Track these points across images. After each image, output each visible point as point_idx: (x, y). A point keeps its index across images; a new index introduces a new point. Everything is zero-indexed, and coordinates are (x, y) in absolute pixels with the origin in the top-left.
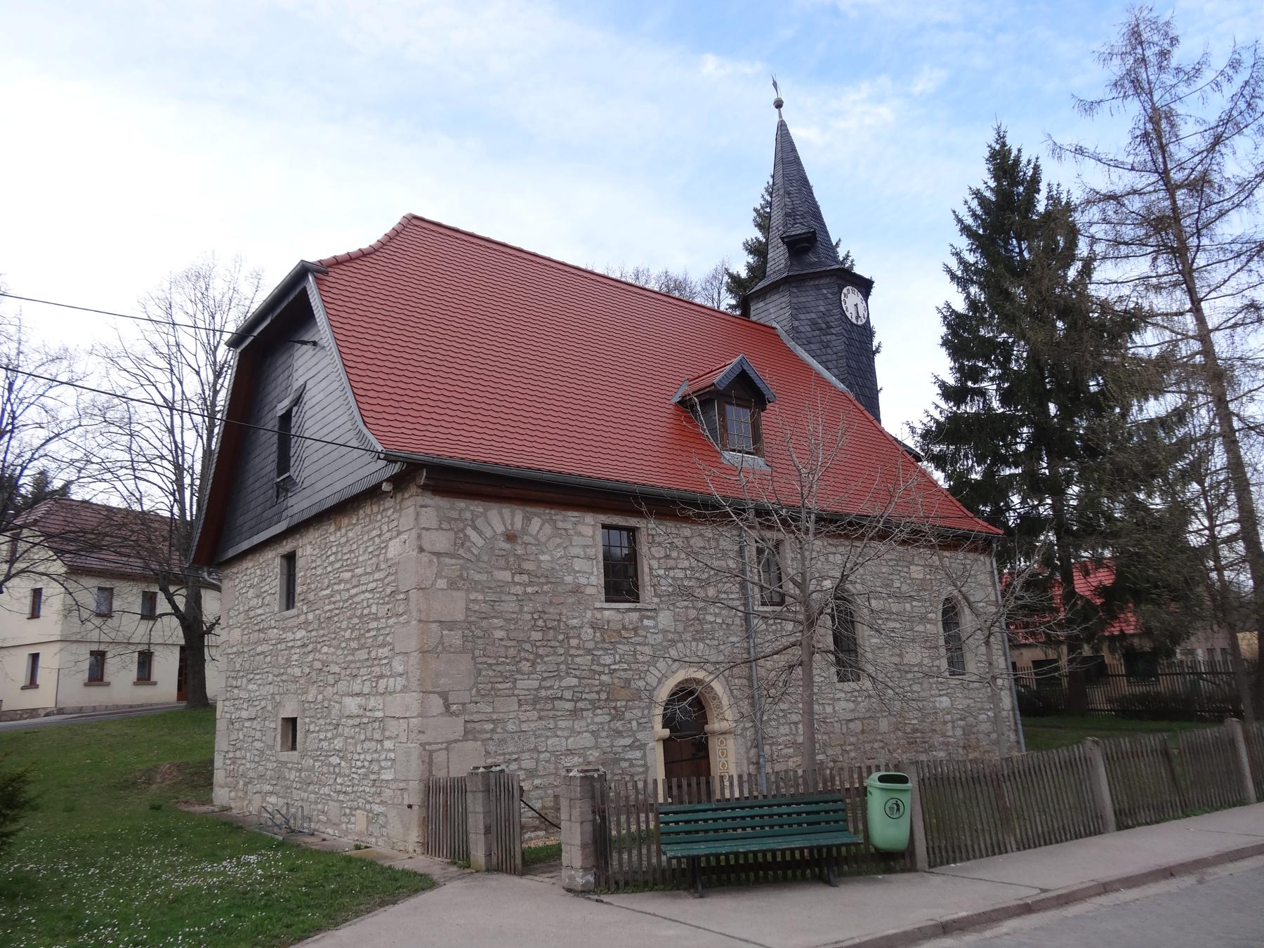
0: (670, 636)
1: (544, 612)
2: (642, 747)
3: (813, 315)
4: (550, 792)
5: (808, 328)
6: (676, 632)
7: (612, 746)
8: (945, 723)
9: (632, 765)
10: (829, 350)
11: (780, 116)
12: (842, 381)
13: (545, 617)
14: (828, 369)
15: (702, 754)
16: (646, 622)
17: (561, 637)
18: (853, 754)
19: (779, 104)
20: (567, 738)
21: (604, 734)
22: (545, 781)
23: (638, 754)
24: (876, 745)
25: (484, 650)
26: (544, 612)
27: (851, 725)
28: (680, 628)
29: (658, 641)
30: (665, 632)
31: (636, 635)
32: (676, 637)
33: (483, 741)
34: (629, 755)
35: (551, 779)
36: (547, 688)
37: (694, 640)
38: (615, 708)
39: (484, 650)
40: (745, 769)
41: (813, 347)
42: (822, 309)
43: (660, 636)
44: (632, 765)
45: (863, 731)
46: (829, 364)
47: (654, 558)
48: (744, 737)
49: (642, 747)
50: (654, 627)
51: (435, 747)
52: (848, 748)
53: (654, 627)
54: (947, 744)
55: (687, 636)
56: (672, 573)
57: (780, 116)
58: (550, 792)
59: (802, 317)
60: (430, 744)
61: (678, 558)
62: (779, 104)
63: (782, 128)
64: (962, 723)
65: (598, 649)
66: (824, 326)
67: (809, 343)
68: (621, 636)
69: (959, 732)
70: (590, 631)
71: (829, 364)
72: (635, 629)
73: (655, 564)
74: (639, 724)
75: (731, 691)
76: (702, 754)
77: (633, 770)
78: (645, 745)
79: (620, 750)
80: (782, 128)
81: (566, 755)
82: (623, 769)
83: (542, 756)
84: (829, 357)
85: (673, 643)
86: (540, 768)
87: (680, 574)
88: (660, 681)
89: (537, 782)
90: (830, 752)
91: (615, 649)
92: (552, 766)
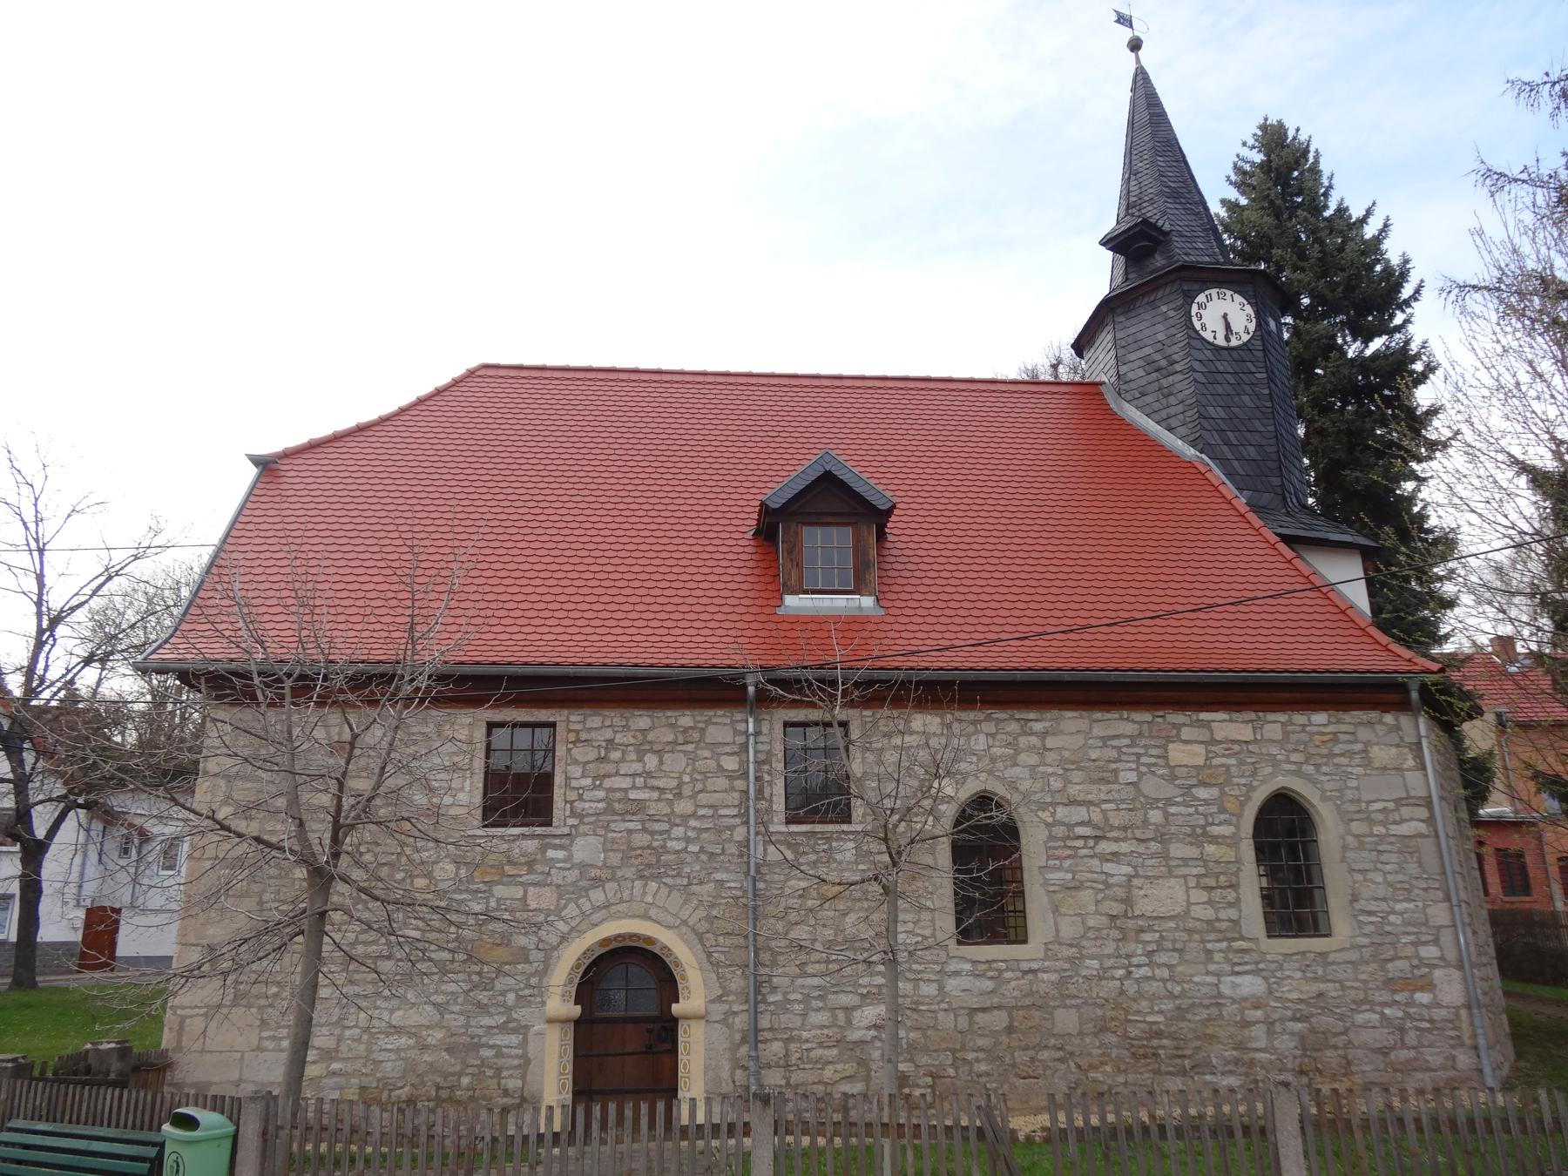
0: (593, 873)
1: (377, 844)
2: (523, 1030)
3: (1147, 351)
4: (355, 1081)
5: (1141, 372)
6: (605, 866)
7: (467, 1026)
8: (1247, 1024)
9: (499, 1054)
10: (1172, 400)
11: (1138, 60)
12: (1193, 444)
13: (378, 850)
14: (1170, 430)
15: (667, 1046)
16: (551, 853)
17: (400, 876)
18: (983, 1067)
19: (1135, 45)
20: (392, 1011)
21: (456, 1008)
22: (349, 1067)
23: (514, 1039)
24: (1045, 1055)
25: (278, 892)
26: (377, 844)
27: (981, 1018)
28: (615, 858)
29: (569, 880)
30: (583, 867)
31: (531, 871)
32: (605, 874)
33: (259, 1008)
34: (498, 1040)
35: (358, 1065)
36: (365, 943)
37: (642, 877)
38: (479, 973)
39: (278, 892)
40: (725, 1074)
41: (1148, 399)
42: (1161, 337)
43: (576, 872)
44: (499, 1054)
45: (1010, 1030)
46: (1174, 422)
47: (576, 762)
48: (729, 1026)
49: (523, 1030)
50: (565, 861)
51: (187, 1012)
52: (970, 1056)
53: (565, 861)
54: (1252, 1063)
55: (629, 873)
56: (608, 783)
57: (1138, 60)
58: (355, 1081)
59: (1132, 357)
60: (183, 1008)
61: (623, 760)
62: (1135, 45)
63: (1143, 86)
64: (1298, 1026)
65: (460, 892)
66: (1163, 363)
67: (1143, 394)
68: (503, 874)
69: (1286, 1044)
70: (451, 867)
71: (1174, 422)
72: (530, 865)
73: (576, 771)
74: (519, 997)
75: (709, 955)
76: (667, 1046)
77: (500, 1062)
78: (527, 1027)
79: (480, 1032)
80: (1143, 86)
81: (388, 1035)
82: (483, 1060)
83: (347, 1033)
84: (1172, 411)
85: (597, 882)
86: (343, 1048)
87: (625, 783)
88: (564, 938)
89: (335, 1066)
90: (924, 1060)
91: (490, 891)
92: (362, 1048)
